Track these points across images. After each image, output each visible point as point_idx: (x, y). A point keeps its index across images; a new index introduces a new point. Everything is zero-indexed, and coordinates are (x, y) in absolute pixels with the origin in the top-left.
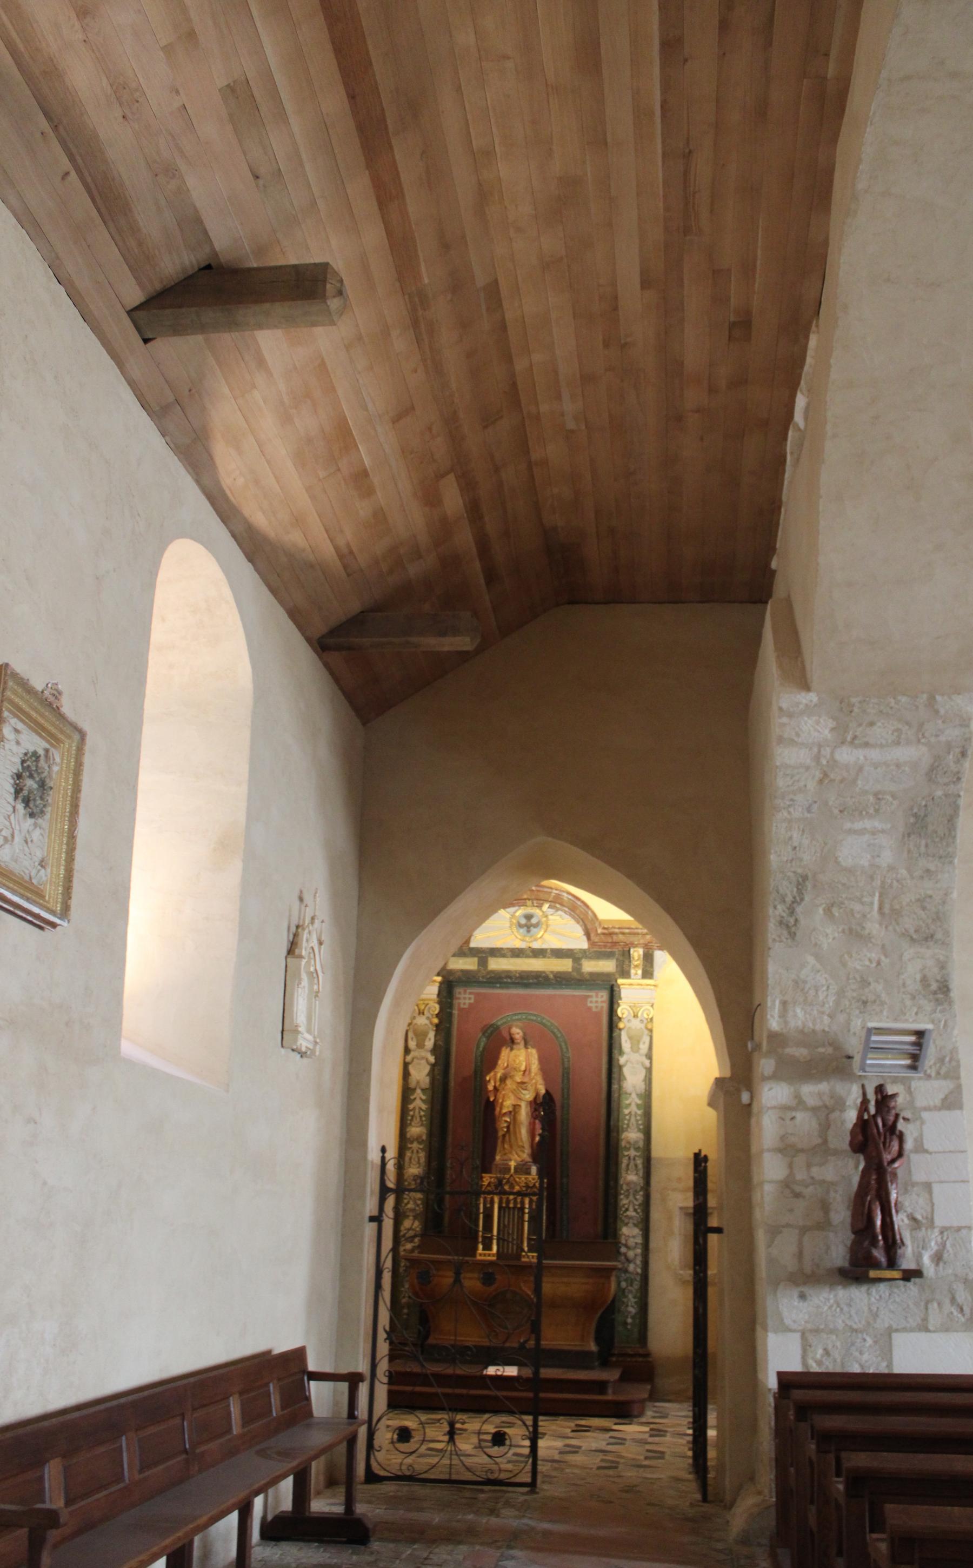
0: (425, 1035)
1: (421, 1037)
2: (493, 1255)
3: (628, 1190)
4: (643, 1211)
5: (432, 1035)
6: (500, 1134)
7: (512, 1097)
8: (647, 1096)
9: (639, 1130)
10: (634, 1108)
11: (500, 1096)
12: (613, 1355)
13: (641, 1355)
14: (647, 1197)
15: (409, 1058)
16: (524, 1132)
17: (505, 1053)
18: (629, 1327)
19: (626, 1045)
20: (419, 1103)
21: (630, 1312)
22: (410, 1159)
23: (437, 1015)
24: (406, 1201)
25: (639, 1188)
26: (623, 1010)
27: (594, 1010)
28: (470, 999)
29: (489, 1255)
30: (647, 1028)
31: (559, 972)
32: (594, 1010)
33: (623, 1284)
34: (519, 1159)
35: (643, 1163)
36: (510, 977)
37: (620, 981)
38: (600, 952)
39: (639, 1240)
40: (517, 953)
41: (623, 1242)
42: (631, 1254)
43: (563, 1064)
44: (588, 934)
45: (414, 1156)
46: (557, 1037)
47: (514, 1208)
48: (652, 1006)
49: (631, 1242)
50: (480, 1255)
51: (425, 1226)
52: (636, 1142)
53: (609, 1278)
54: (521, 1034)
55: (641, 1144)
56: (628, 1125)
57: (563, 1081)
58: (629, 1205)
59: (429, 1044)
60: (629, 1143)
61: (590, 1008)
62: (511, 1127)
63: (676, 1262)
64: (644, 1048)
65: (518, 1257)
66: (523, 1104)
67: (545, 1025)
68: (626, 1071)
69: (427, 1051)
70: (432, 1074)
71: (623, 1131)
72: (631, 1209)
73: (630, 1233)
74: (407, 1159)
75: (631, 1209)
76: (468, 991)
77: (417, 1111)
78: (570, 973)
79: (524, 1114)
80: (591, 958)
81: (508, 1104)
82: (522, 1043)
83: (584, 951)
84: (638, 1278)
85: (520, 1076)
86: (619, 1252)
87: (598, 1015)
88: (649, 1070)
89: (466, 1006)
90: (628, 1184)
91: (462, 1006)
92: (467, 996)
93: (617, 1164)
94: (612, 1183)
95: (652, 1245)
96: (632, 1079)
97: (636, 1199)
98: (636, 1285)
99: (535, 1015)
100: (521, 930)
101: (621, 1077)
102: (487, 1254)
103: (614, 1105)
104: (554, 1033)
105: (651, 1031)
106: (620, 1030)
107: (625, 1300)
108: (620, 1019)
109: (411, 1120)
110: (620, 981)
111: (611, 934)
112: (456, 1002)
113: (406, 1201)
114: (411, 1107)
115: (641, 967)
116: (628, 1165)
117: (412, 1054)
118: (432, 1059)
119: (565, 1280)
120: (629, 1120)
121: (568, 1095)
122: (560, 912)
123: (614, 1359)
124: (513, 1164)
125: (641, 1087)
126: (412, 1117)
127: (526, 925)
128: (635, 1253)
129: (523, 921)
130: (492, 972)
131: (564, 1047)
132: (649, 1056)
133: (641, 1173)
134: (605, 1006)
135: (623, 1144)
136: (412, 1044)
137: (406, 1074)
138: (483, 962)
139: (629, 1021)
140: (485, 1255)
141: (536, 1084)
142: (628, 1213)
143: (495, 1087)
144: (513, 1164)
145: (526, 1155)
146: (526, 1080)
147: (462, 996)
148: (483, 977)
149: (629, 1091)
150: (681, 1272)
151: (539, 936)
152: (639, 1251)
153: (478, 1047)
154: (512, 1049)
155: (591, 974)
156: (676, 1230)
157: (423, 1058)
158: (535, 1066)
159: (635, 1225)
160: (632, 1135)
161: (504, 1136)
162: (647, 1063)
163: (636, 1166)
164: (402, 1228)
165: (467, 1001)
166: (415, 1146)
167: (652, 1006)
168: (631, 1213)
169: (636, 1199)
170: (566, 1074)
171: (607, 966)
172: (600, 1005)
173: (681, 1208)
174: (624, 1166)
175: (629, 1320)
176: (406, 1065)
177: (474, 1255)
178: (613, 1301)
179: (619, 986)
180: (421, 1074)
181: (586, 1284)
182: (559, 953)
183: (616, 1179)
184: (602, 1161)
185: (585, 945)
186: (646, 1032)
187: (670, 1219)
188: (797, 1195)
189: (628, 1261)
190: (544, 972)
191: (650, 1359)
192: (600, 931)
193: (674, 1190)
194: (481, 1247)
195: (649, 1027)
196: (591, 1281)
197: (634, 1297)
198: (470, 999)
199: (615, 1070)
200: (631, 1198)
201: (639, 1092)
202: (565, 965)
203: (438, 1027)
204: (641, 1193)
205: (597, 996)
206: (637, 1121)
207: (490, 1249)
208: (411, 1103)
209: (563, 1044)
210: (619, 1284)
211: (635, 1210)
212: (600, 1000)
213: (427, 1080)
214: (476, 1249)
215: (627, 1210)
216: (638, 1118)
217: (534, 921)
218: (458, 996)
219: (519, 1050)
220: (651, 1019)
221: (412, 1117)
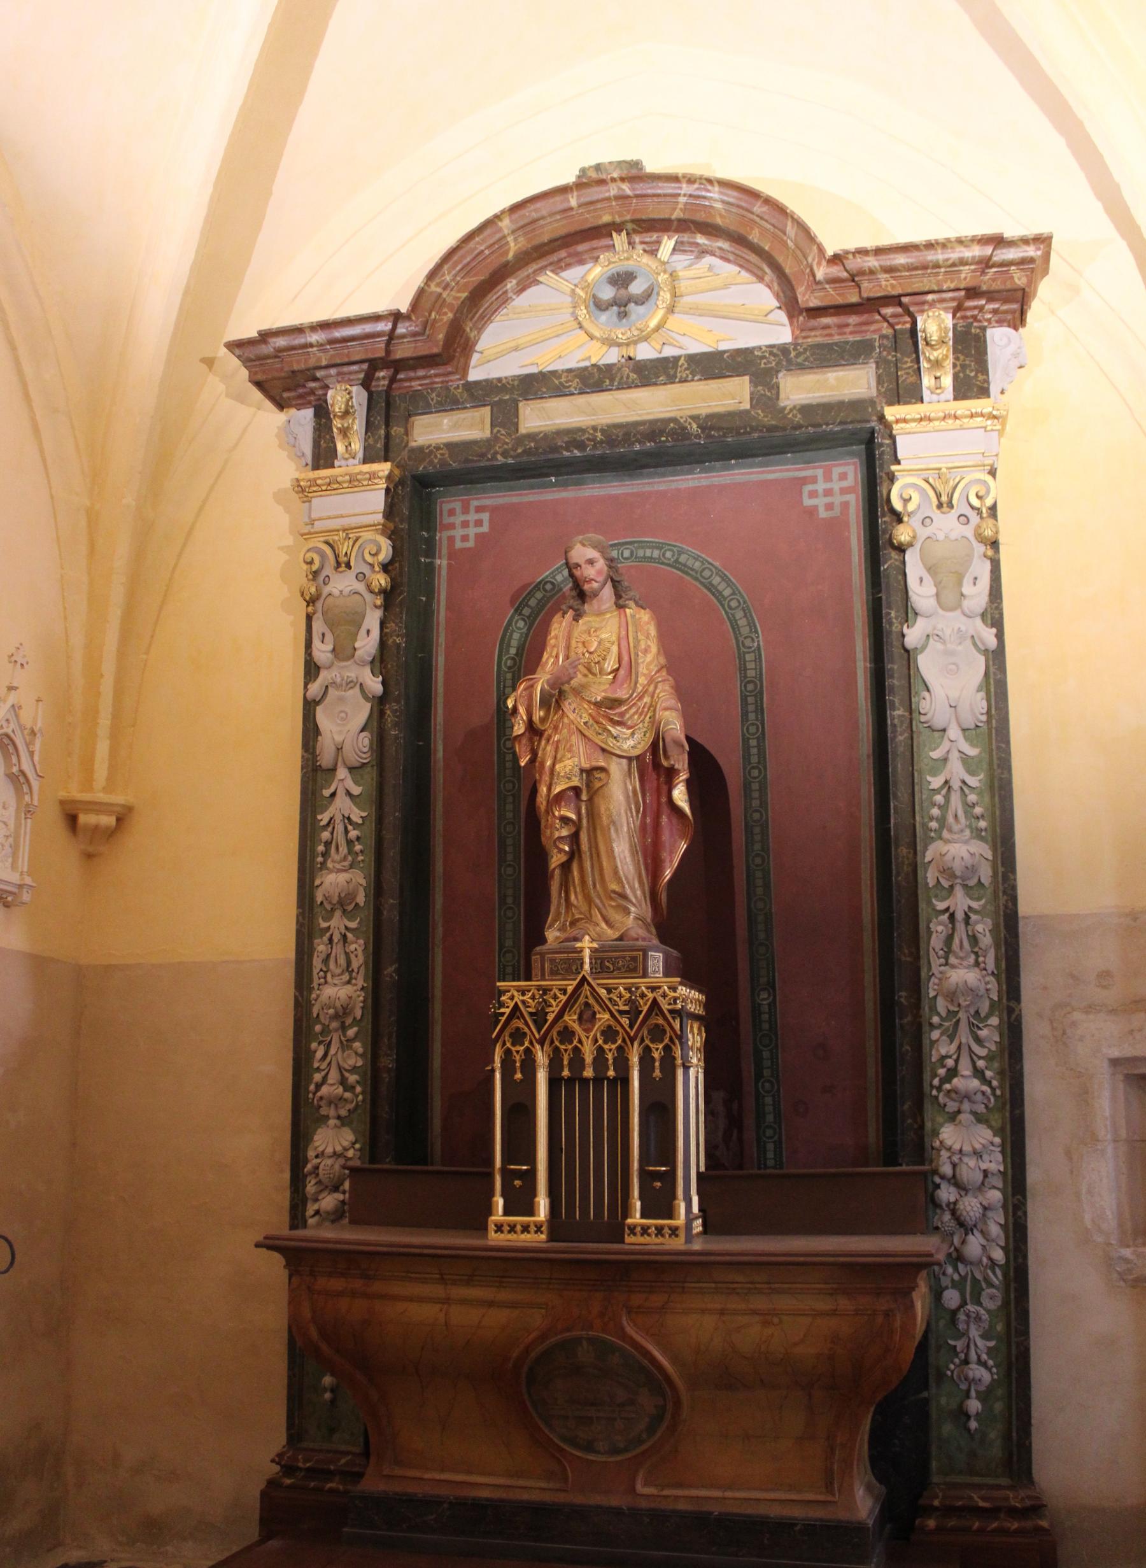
0: (356, 620)
1: (345, 625)
2: (539, 1229)
3: (951, 1014)
4: (1001, 1073)
5: (373, 620)
6: (556, 860)
7: (581, 748)
8: (995, 730)
9: (978, 834)
10: (956, 770)
11: (547, 752)
12: (929, 1510)
13: (1014, 1512)
14: (1013, 1033)
15: (315, 688)
16: (622, 851)
17: (559, 627)
18: (973, 1425)
19: (921, 590)
20: (347, 803)
21: (971, 1381)
22: (326, 961)
23: (386, 568)
24: (318, 1077)
25: (985, 1007)
26: (904, 490)
27: (823, 514)
28: (479, 523)
29: (526, 1229)
30: (981, 538)
31: (710, 416)
32: (823, 514)
33: (951, 1298)
34: (611, 934)
35: (994, 931)
36: (581, 446)
37: (891, 413)
38: (829, 347)
39: (995, 1163)
40: (594, 380)
41: (947, 1169)
42: (970, 1206)
43: (743, 669)
44: (791, 306)
45: (338, 950)
46: (718, 595)
47: (598, 1080)
48: (993, 473)
49: (970, 1171)
50: (499, 1228)
51: (373, 1147)
52: (972, 869)
53: (905, 1294)
54: (601, 564)
55: (985, 874)
56: (942, 821)
57: (745, 715)
58: (957, 1059)
59: (367, 644)
60: (948, 872)
61: (812, 511)
62: (584, 837)
63: (1110, 1222)
64: (977, 595)
65: (616, 1230)
66: (617, 769)
67: (684, 568)
68: (926, 664)
69: (362, 664)
70: (377, 724)
71: (928, 841)
72: (965, 1069)
73: (964, 1143)
74: (317, 963)
75: (965, 1069)
76: (474, 503)
77: (340, 828)
78: (746, 412)
79: (620, 793)
80: (802, 367)
81: (565, 765)
82: (608, 592)
83: (784, 349)
84: (997, 1278)
85: (608, 696)
86: (935, 1204)
87: (836, 526)
88: (996, 658)
89: (471, 544)
90: (951, 996)
91: (459, 545)
92: (472, 517)
93: (916, 939)
94: (903, 996)
95: (1034, 1176)
96: (947, 684)
97: (979, 1041)
98: (992, 1299)
99: (659, 547)
100: (604, 317)
101: (912, 679)
102: (518, 1228)
103: (898, 767)
104: (710, 587)
105: (994, 544)
106: (901, 549)
107: (959, 1345)
108: (898, 518)
109: (325, 855)
110: (891, 413)
111: (854, 278)
112: (442, 536)
113: (318, 1077)
114: (324, 818)
115: (948, 364)
116: (949, 939)
117: (324, 676)
118: (375, 685)
119: (760, 1303)
120: (944, 808)
121: (762, 754)
122: (708, 260)
123: (931, 1523)
124: (586, 945)
125: (975, 705)
126: (328, 844)
127: (614, 302)
128: (983, 1203)
129: (607, 293)
130: (531, 437)
131: (742, 622)
132: (994, 616)
133: (990, 962)
134: (855, 502)
135: (931, 877)
136: (322, 651)
137: (311, 732)
138: (505, 416)
139: (926, 521)
140: (512, 1228)
141: (652, 706)
142: (325, 1090)
143: (530, 724)
144: (586, 945)
145: (633, 919)
146: (622, 694)
147: (459, 519)
148: (505, 454)
149: (938, 723)
150: (1127, 1253)
151: (653, 324)
152: (995, 1196)
153: (504, 645)
154: (577, 617)
155: (806, 410)
156: (1104, 1132)
157: (350, 684)
158: (649, 660)
159: (979, 1119)
160: (956, 849)
161: (566, 867)
162: (989, 636)
163: (974, 940)
164: (311, 1154)
165: (472, 531)
166: (337, 923)
167: (993, 473)
168: (966, 1082)
169: (979, 1041)
170: (753, 698)
171: (854, 382)
172: (838, 499)
173: (1115, 1062)
174: (936, 942)
175: (974, 1405)
176: (310, 706)
177: (482, 1227)
178: (923, 1347)
179: (888, 426)
180: (346, 727)
181: (834, 1313)
182: (711, 366)
183: (916, 987)
184: (869, 941)
185: (781, 333)
186: (980, 549)
187: (1084, 1096)
188: (317, 1157)
189: (965, 1227)
190: (674, 420)
191: (1044, 1524)
192: (820, 274)
193: (1089, 1009)
194: (499, 1202)
195: (988, 533)
196: (844, 1303)
197: (985, 1336)
198: (479, 523)
199: (894, 667)
200: (964, 1035)
201: (970, 723)
202: (732, 395)
203: (389, 596)
204: (994, 1021)
205: (828, 477)
206: (969, 807)
207: (531, 1211)
208: (324, 809)
209: (739, 614)
210: (937, 1294)
211: (978, 1073)
212: (836, 486)
213: (365, 740)
214: (489, 1210)
215: (953, 1073)
216: (972, 798)
217: (636, 288)
218: (447, 520)
219: (600, 614)
220: (993, 509)
221: (328, 844)
